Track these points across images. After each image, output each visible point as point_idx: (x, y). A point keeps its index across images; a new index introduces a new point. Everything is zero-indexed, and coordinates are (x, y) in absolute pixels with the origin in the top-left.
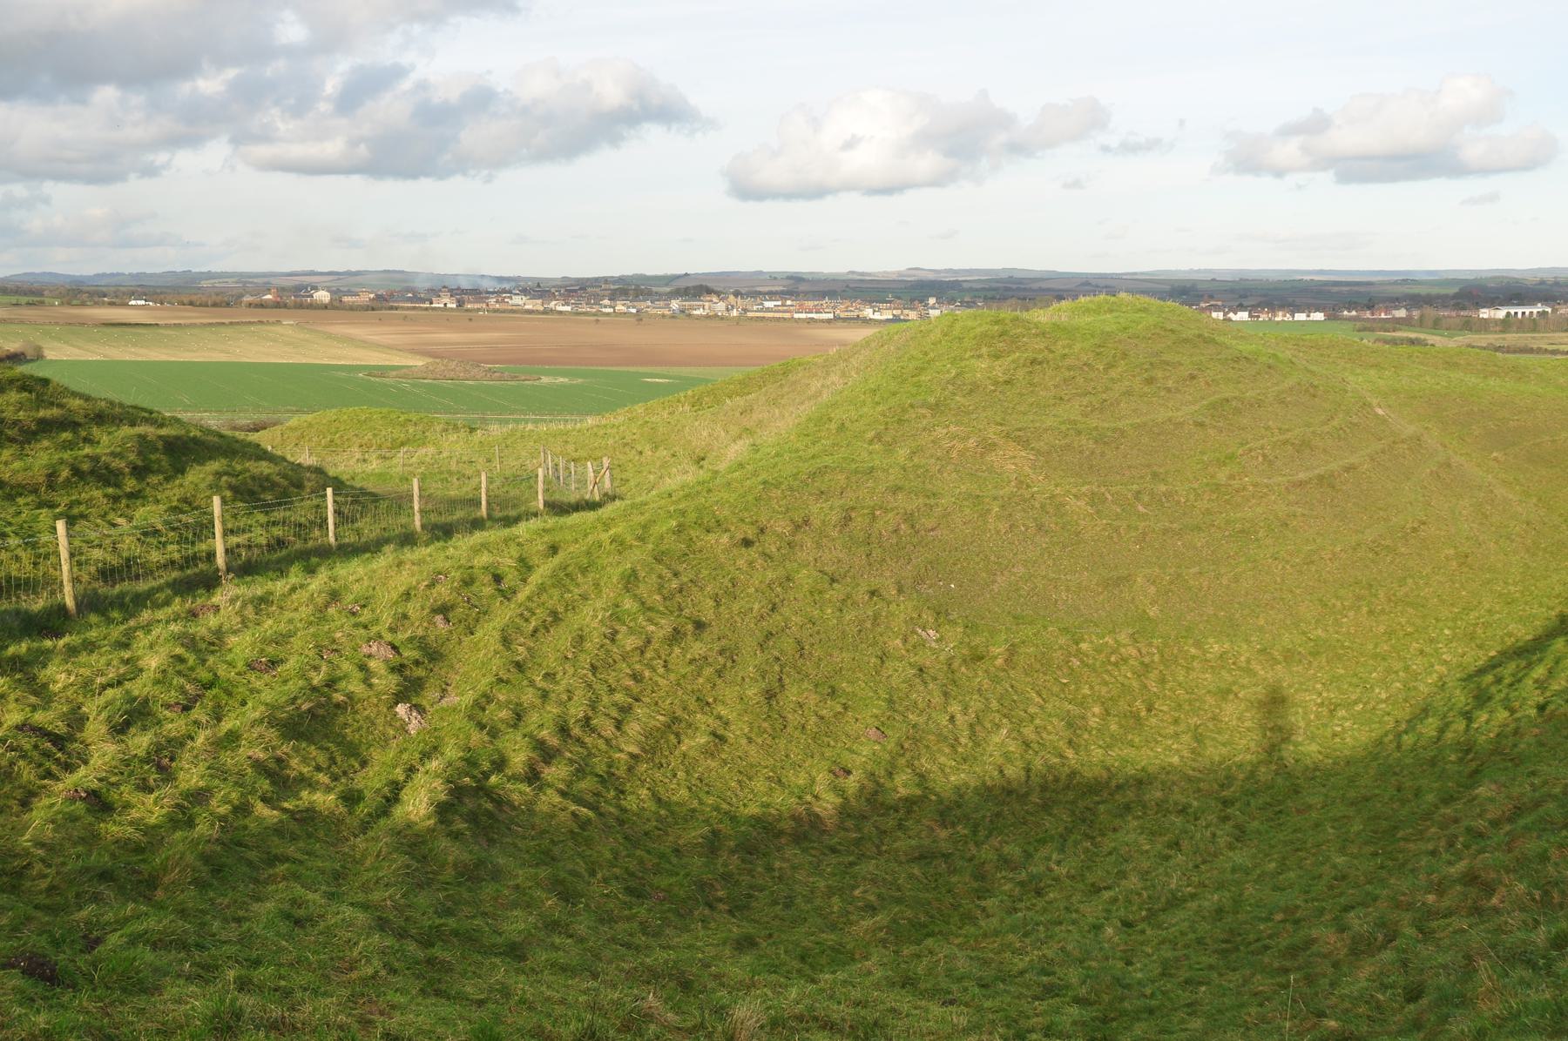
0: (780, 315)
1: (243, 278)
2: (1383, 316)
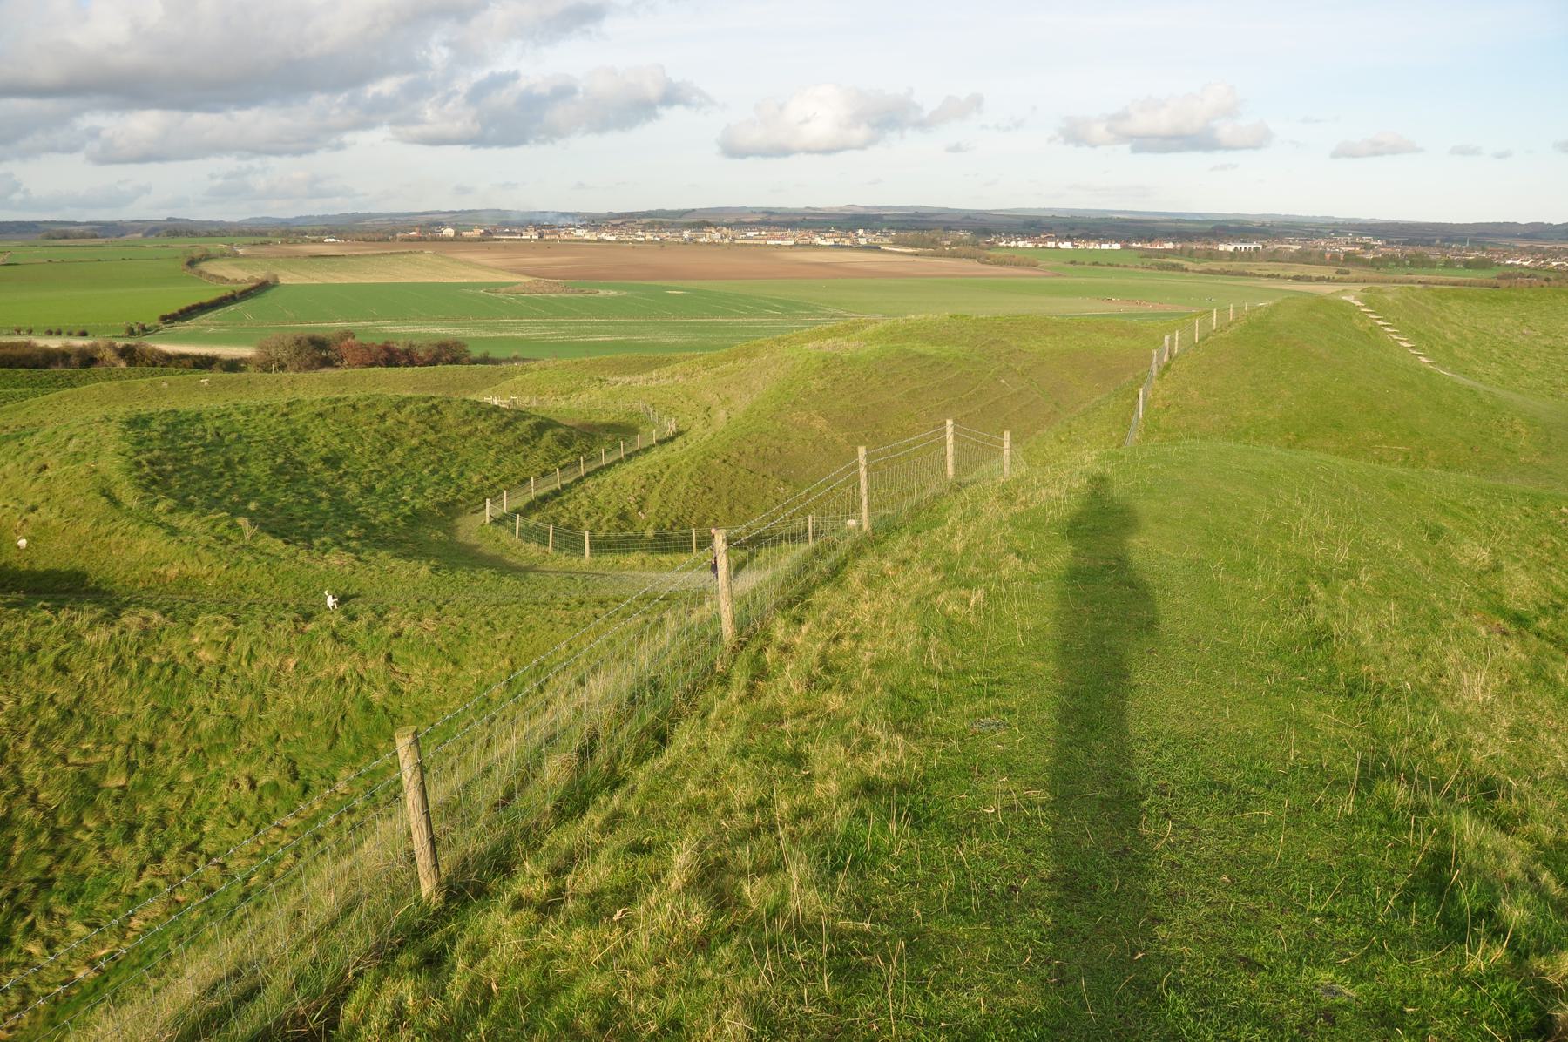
0: (756, 242)
1: (392, 217)
2: (1158, 247)
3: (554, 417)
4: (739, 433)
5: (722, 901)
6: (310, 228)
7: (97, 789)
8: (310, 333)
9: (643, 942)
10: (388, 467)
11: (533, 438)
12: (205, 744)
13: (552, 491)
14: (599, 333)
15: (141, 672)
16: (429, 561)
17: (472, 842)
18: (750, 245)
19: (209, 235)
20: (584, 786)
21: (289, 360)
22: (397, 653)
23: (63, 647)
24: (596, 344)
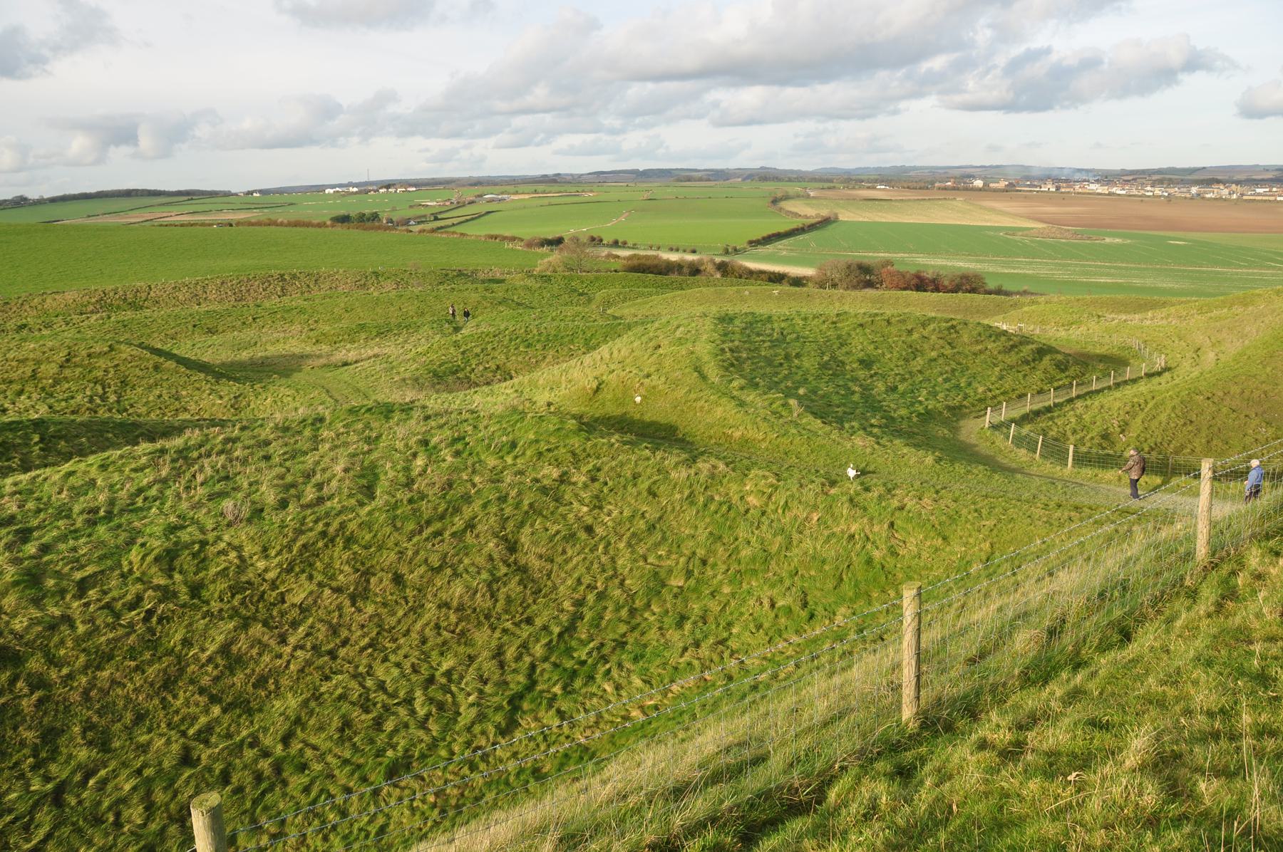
0: (1267, 198)
1: (933, 170)
3: (1054, 344)
4: (1226, 374)
5: (1175, 790)
6: (866, 177)
7: (664, 585)
8: (860, 260)
9: (1095, 805)
10: (910, 373)
11: (1034, 360)
12: (743, 567)
13: (1045, 407)
14: (1102, 275)
15: (705, 505)
16: (933, 453)
17: (951, 684)
18: (1259, 201)
19: (790, 180)
20: (1050, 661)
21: (841, 280)
22: (898, 523)
23: (655, 478)
24: (1098, 285)
